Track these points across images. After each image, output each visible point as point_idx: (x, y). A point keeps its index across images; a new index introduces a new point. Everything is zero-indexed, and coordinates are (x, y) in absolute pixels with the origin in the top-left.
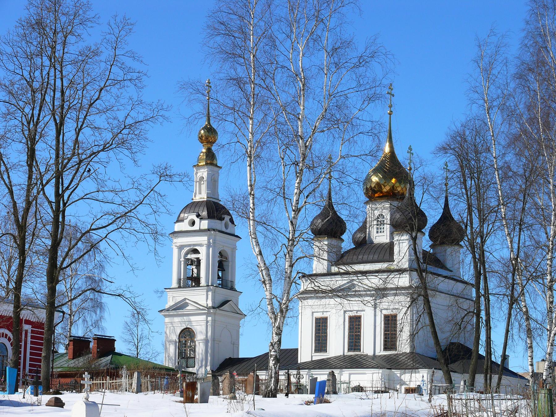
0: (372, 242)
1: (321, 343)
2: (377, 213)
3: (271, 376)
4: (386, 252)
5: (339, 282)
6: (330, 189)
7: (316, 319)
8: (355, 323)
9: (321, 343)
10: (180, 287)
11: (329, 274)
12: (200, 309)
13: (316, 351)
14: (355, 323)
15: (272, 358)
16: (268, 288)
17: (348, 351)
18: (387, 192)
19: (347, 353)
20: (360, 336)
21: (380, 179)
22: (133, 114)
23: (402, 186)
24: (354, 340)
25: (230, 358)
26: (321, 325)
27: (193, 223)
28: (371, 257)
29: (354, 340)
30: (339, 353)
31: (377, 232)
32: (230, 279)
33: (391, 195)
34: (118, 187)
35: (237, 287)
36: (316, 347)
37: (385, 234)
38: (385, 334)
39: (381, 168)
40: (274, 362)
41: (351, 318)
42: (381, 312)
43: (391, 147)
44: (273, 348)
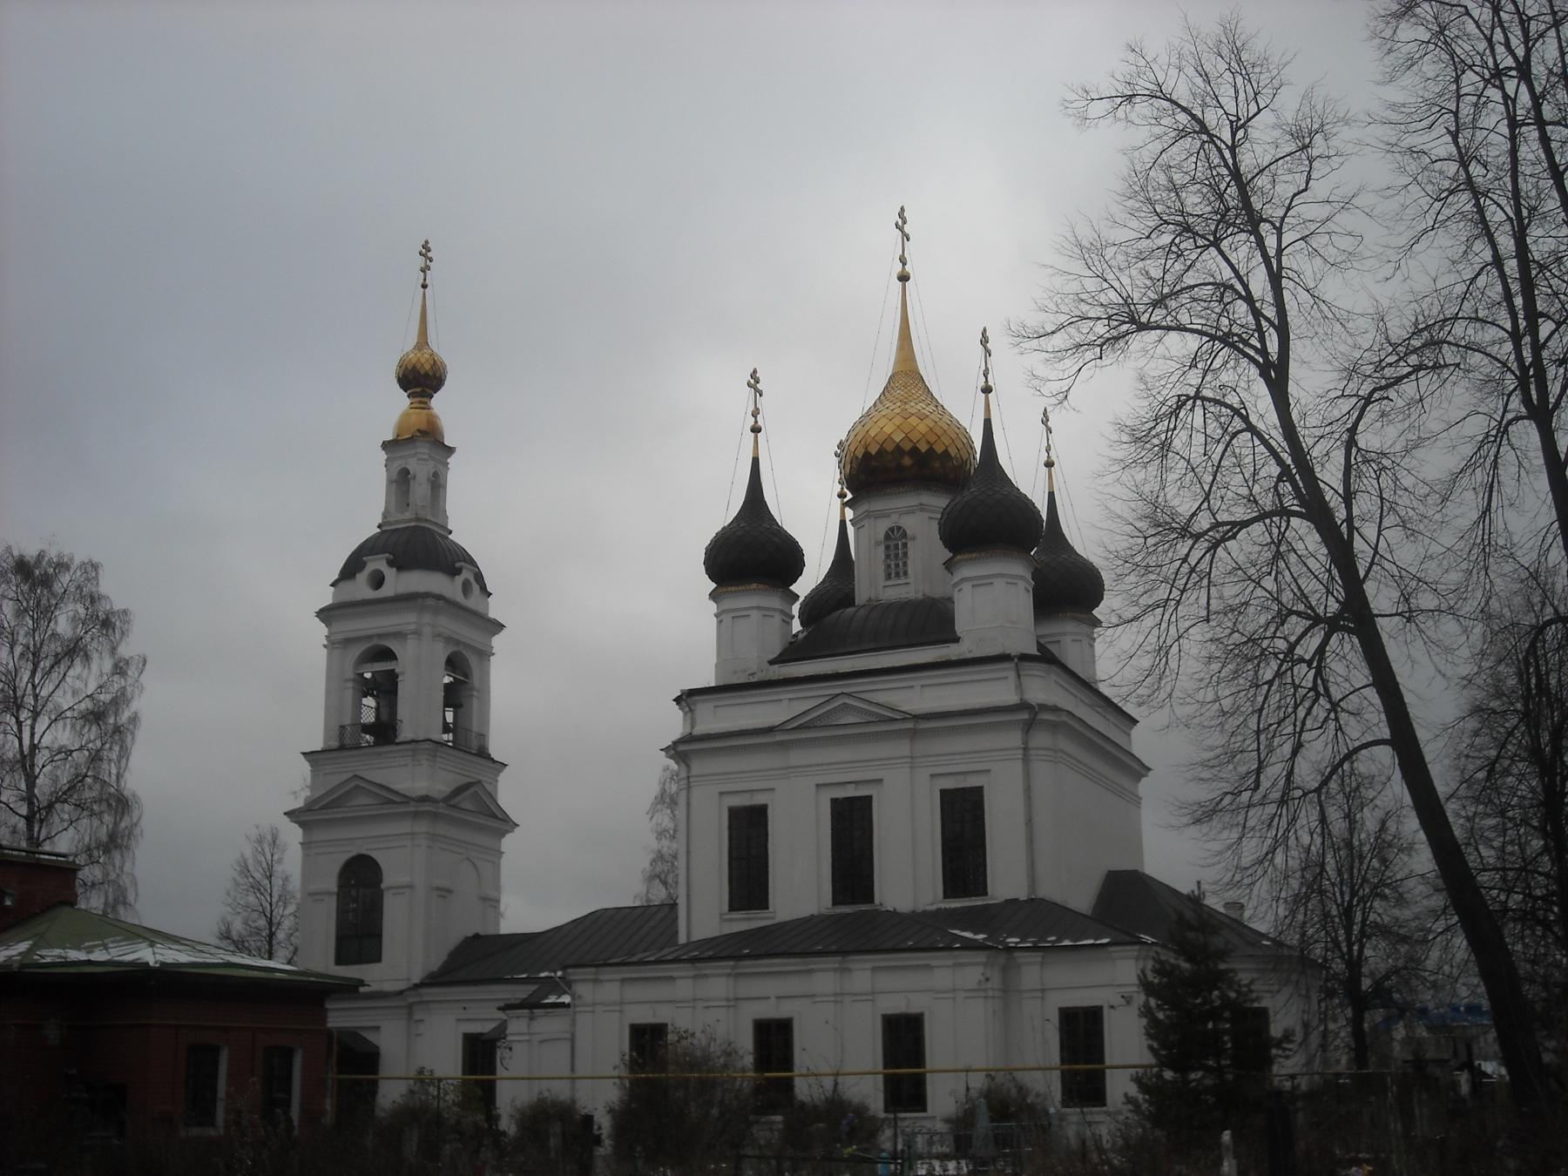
4: (930, 622)
6: (756, 462)
8: (852, 824)
10: (342, 748)
12: (394, 802)
14: (852, 824)
25: (477, 936)
27: (378, 581)
32: (475, 728)
35: (495, 751)
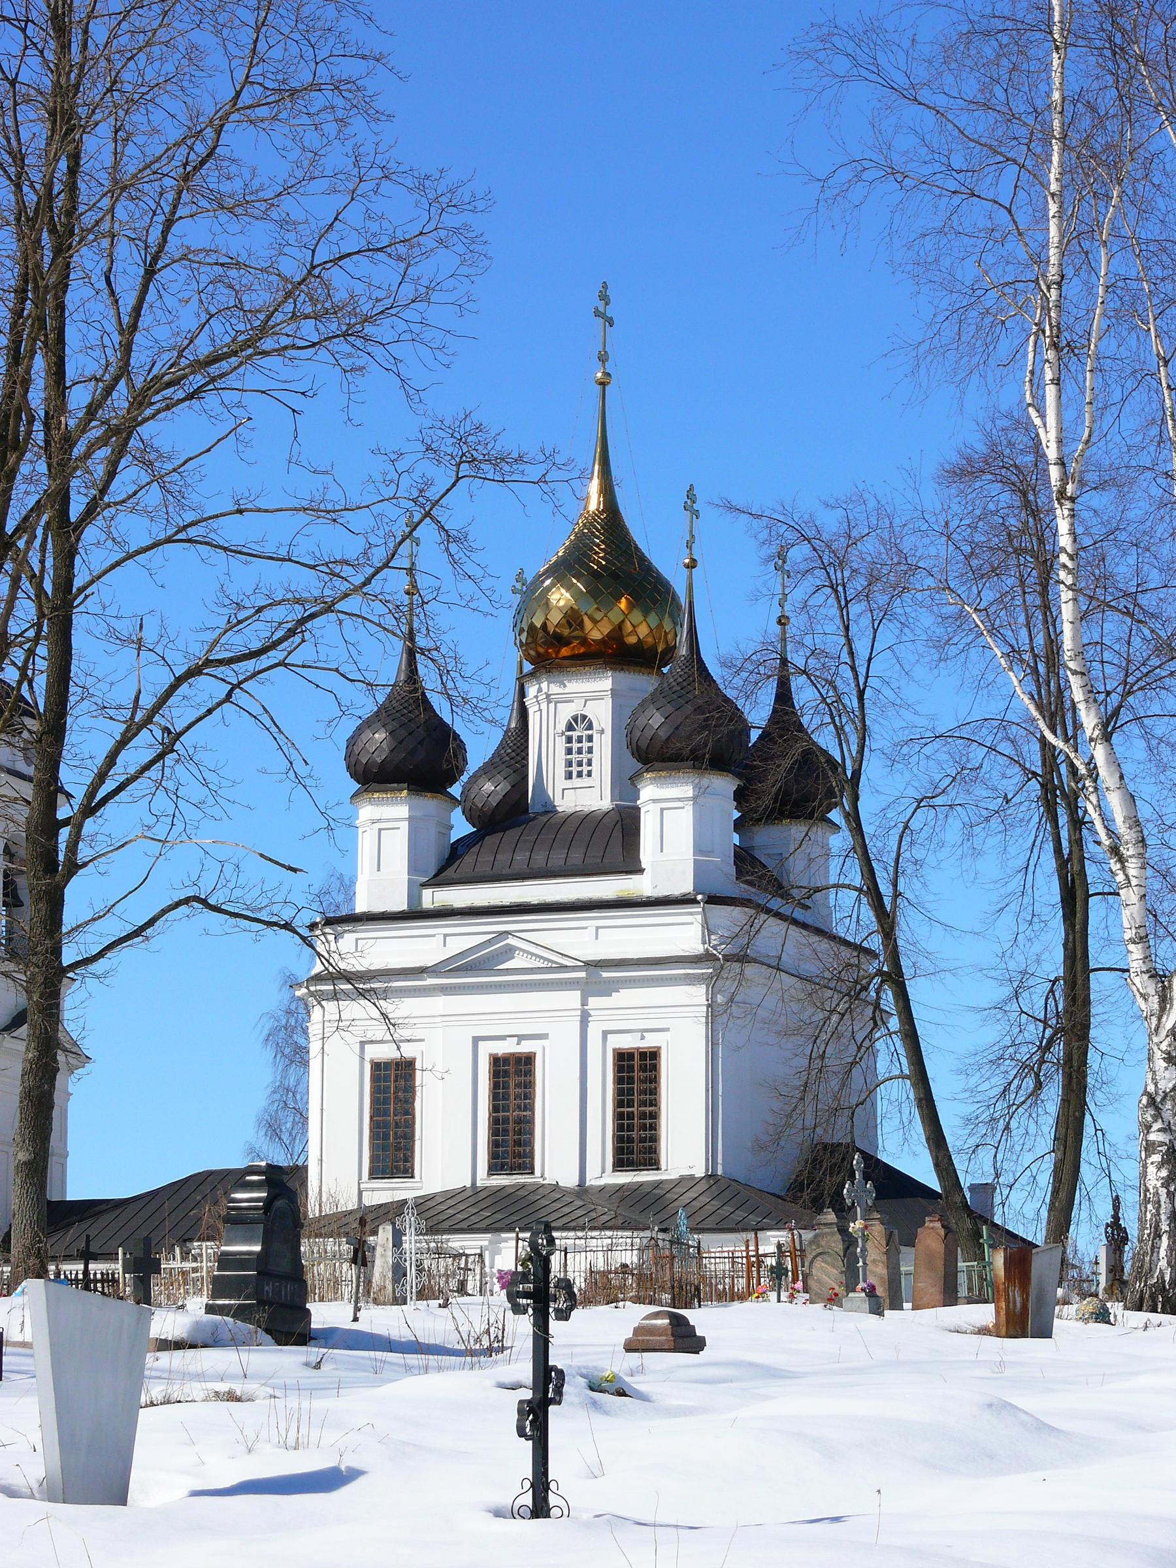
0: (549, 809)
1: (392, 1147)
2: (566, 712)
3: (1157, 1227)
4: (613, 840)
5: (461, 938)
7: (377, 1066)
8: (512, 1079)
9: (392, 1147)
11: (415, 914)
13: (375, 1174)
14: (512, 1079)
15: (1156, 1158)
16: (1132, 872)
17: (490, 1174)
18: (603, 641)
19: (484, 1179)
20: (531, 1121)
21: (577, 595)
22: (354, 214)
23: (653, 619)
24: (511, 1139)
26: (392, 1090)
28: (576, 857)
29: (511, 1139)
30: (459, 1179)
31: (569, 776)
33: (617, 654)
34: (335, 497)
36: (373, 1159)
37: (594, 780)
38: (619, 1116)
39: (579, 561)
40: (1164, 1173)
41: (497, 1062)
42: (605, 1039)
43: (607, 490)
44: (1158, 1116)
